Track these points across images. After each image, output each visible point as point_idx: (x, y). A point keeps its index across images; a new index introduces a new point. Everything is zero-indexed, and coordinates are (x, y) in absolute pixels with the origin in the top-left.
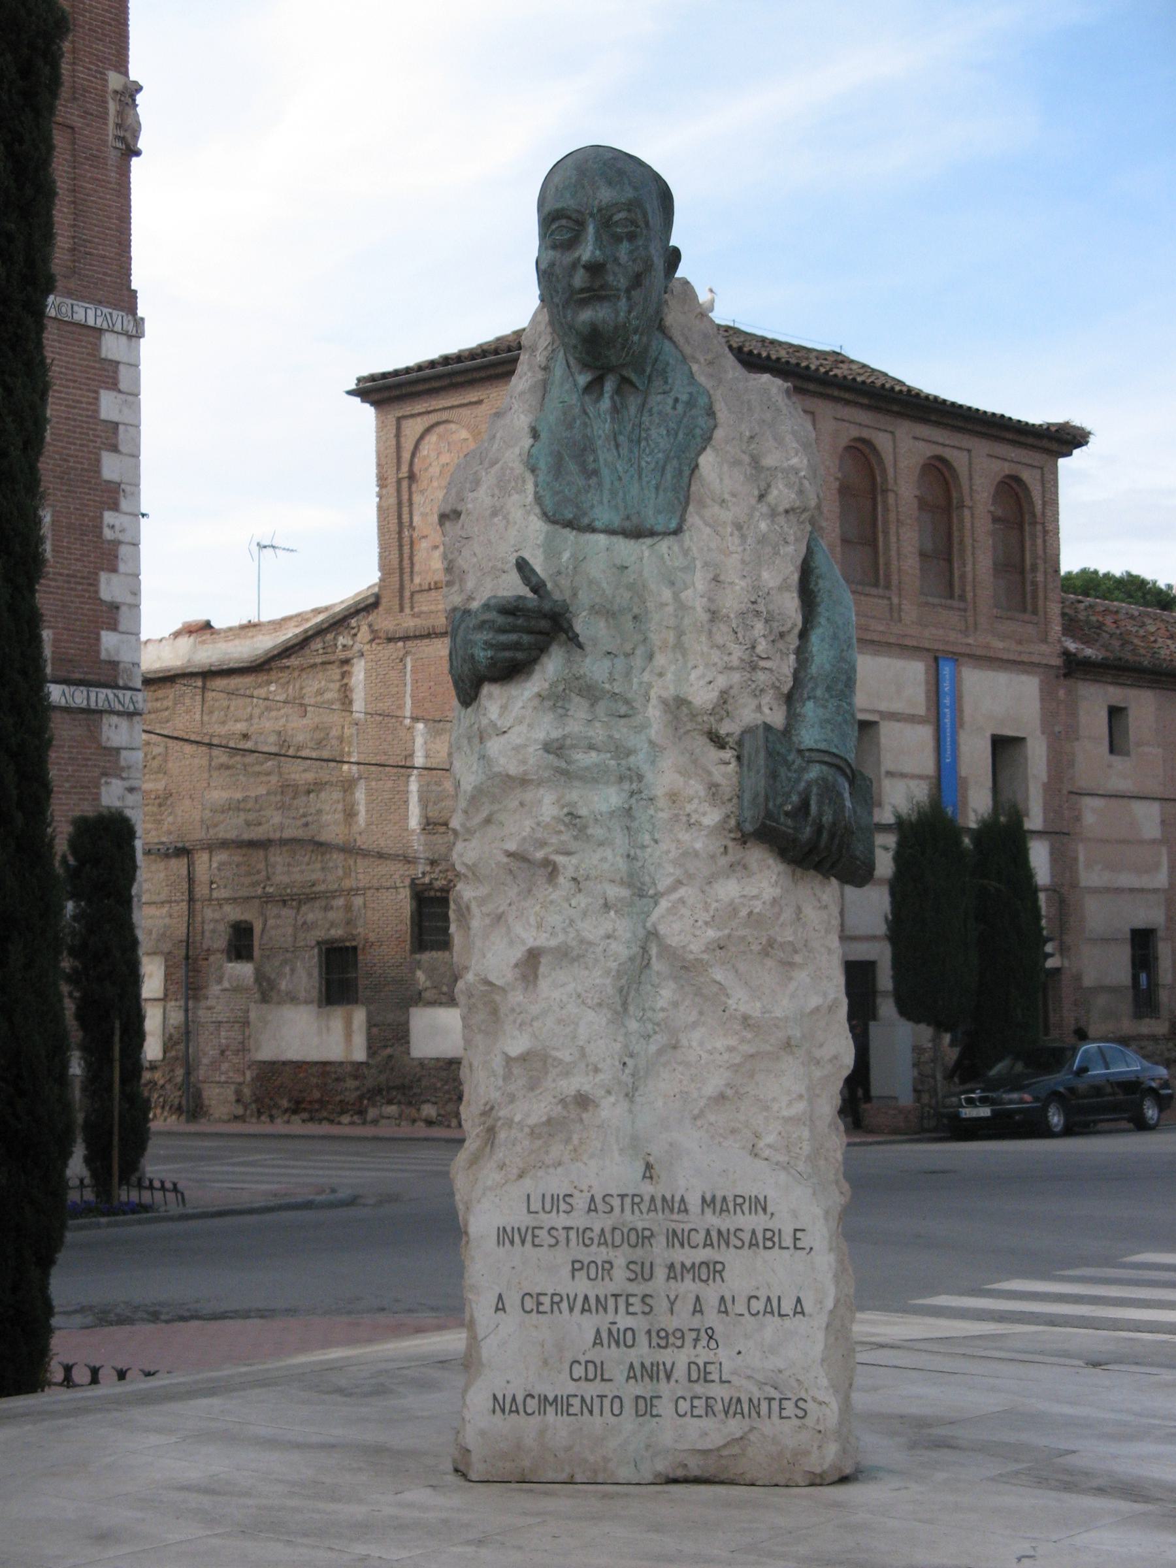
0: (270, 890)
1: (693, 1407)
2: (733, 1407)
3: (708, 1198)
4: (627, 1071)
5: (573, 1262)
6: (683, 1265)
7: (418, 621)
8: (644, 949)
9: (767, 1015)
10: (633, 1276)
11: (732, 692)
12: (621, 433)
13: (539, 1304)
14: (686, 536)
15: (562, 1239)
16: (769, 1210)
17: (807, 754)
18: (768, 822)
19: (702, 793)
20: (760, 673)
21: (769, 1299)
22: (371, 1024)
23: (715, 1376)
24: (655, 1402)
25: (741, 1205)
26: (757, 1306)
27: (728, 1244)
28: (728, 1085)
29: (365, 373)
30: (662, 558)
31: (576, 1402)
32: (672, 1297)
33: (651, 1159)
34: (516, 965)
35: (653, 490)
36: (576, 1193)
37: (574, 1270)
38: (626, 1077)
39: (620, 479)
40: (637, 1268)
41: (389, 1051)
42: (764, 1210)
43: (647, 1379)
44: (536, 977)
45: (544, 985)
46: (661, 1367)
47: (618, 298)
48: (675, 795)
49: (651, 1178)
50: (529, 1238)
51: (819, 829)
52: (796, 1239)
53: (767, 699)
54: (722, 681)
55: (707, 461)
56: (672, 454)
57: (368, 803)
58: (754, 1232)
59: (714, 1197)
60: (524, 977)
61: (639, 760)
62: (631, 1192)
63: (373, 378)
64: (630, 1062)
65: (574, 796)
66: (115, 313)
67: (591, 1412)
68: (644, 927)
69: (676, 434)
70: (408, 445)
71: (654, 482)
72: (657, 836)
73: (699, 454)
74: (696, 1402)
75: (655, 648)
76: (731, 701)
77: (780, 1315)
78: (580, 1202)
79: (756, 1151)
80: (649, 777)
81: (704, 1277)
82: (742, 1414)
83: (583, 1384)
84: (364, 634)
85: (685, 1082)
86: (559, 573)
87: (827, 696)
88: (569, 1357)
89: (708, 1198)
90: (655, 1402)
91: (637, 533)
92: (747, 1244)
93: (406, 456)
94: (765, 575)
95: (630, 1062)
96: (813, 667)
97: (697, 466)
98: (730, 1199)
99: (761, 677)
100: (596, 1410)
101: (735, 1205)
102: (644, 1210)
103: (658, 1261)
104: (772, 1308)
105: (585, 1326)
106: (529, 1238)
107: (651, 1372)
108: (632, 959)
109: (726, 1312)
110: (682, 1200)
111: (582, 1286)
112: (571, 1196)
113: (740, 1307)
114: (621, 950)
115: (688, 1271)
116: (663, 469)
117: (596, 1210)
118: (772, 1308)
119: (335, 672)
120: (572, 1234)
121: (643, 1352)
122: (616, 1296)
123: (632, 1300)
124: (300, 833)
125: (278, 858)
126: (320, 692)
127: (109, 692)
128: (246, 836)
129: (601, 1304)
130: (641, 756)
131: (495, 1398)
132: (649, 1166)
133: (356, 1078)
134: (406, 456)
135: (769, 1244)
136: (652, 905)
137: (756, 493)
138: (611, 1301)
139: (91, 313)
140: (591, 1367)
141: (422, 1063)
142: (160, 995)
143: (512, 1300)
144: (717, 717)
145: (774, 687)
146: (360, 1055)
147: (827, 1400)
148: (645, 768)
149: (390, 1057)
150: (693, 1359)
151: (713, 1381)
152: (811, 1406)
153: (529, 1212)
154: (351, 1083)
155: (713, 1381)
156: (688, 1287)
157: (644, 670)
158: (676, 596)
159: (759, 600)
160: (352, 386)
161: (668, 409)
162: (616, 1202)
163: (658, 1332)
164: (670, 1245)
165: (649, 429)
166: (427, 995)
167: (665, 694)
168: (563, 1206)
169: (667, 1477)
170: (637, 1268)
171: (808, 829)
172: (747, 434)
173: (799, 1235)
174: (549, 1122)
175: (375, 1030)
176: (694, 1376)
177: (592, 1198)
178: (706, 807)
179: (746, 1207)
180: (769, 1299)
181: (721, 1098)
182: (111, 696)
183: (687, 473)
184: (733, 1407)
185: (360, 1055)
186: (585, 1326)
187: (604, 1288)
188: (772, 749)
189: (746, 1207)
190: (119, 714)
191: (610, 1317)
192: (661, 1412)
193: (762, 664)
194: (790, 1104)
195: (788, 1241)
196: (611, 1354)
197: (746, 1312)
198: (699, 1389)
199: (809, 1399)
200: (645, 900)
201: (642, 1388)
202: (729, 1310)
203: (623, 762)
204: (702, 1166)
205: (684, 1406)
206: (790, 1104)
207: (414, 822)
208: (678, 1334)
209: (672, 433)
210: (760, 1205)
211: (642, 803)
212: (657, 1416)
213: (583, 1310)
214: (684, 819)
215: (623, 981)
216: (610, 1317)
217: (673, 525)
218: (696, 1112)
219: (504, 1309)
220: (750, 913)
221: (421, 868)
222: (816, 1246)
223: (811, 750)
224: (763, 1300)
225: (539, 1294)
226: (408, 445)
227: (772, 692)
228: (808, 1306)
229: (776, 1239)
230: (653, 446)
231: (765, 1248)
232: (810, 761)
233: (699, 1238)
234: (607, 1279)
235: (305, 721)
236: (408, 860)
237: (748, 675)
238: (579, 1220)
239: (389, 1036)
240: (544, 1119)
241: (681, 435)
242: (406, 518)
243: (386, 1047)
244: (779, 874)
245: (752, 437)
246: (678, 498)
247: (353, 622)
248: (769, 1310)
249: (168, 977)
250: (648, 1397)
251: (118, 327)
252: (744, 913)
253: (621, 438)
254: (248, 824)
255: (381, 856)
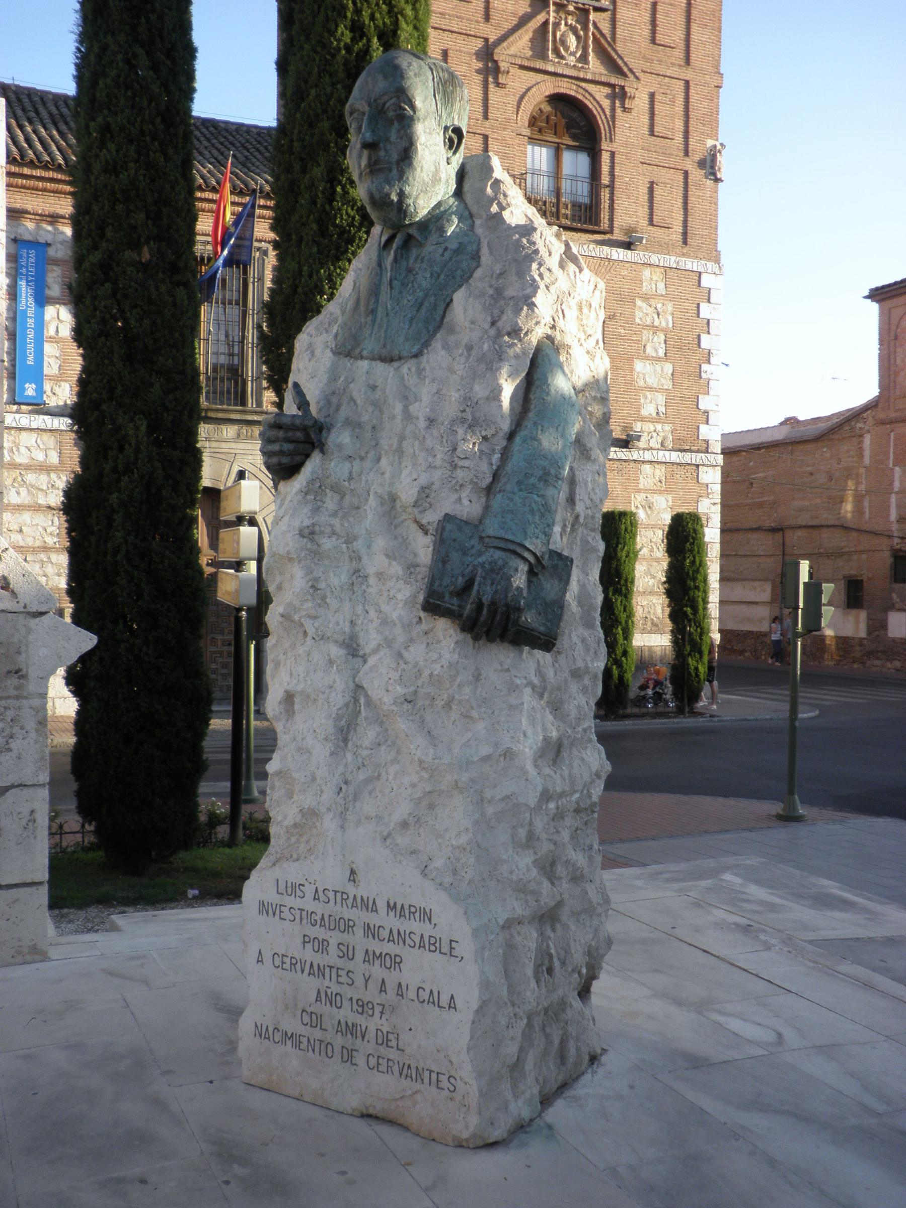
0: (821, 550)
1: (378, 1064)
2: (405, 1071)
3: (392, 905)
4: (341, 795)
5: (304, 936)
6: (374, 953)
7: (898, 414)
8: (356, 700)
9: (436, 761)
10: (341, 955)
11: (434, 487)
12: (396, 279)
13: (283, 963)
14: (424, 359)
15: (298, 917)
16: (433, 922)
17: (487, 540)
18: (431, 601)
19: (401, 573)
20: (459, 471)
21: (431, 991)
22: (869, 619)
23: (393, 1043)
24: (354, 1053)
25: (414, 913)
26: (425, 995)
27: (404, 942)
28: (410, 814)
29: (874, 287)
30: (403, 379)
31: (304, 1040)
32: (367, 976)
33: (354, 866)
34: (280, 703)
35: (407, 323)
36: (306, 884)
37: (304, 942)
38: (340, 800)
39: (387, 315)
40: (344, 949)
41: (877, 633)
42: (430, 920)
43: (349, 1035)
44: (294, 712)
45: (299, 717)
46: (359, 1028)
47: (390, 170)
48: (381, 573)
49: (354, 881)
50: (278, 912)
51: (480, 606)
52: (451, 948)
53: (465, 493)
54: (424, 479)
55: (459, 297)
56: (431, 292)
57: (870, 507)
58: (422, 936)
59: (395, 903)
60: (287, 711)
61: (359, 545)
62: (341, 890)
63: (877, 289)
64: (344, 787)
65: (318, 573)
66: (708, 263)
67: (313, 1050)
68: (354, 682)
69: (439, 276)
70: (894, 321)
71: (409, 316)
72: (367, 607)
73: (454, 292)
74: (381, 1060)
75: (383, 452)
76: (433, 495)
77: (439, 1006)
78: (309, 891)
79: (426, 871)
80: (365, 559)
81: (388, 965)
82: (411, 1077)
83: (308, 1027)
84: (870, 421)
85: (381, 808)
86: (334, 393)
87: (516, 489)
88: (300, 1006)
89: (392, 905)
90: (354, 1053)
91: (388, 359)
92: (417, 945)
93: (893, 327)
94: (477, 388)
95: (344, 787)
96: (510, 465)
97: (452, 300)
98: (406, 907)
99: (460, 474)
100: (317, 1051)
101: (410, 912)
102: (350, 906)
103: (357, 948)
104: (433, 1000)
105: (310, 986)
106: (278, 912)
107: (350, 1029)
108: (347, 705)
109: (402, 996)
110: (374, 902)
111: (308, 955)
112: (303, 885)
113: (412, 994)
114: (339, 699)
115: (378, 958)
116: (421, 305)
117: (319, 899)
118: (433, 1000)
119: (855, 440)
120: (304, 913)
121: (346, 1014)
122: (331, 967)
123: (340, 972)
124: (836, 523)
125: (825, 534)
126: (848, 451)
127: (703, 455)
128: (810, 524)
129: (321, 971)
130: (361, 541)
131: (256, 1026)
132: (353, 872)
133: (860, 645)
134: (893, 327)
135: (433, 948)
136: (361, 663)
137: (489, 319)
138: (327, 970)
139: (695, 264)
140: (314, 1017)
141: (893, 640)
142: (768, 600)
143: (267, 956)
144: (420, 509)
145: (471, 482)
146: (863, 634)
147: (470, 1081)
148: (363, 552)
149: (878, 636)
150: (380, 1027)
151: (392, 1047)
152: (459, 1084)
153: (278, 893)
154: (858, 648)
155: (392, 1047)
156: (377, 972)
157: (371, 470)
158: (406, 409)
159: (467, 409)
160: (867, 293)
161: (437, 256)
162: (331, 895)
163: (358, 1000)
164: (366, 935)
165: (417, 274)
166: (897, 606)
167: (380, 490)
168: (299, 893)
169: (362, 1112)
170: (344, 949)
171: (469, 606)
172: (498, 272)
173: (454, 945)
174: (295, 825)
175: (871, 622)
176: (380, 1041)
177: (317, 891)
178: (401, 584)
179: (417, 915)
180: (431, 991)
181: (404, 825)
182: (704, 457)
183: (442, 307)
184: (405, 1071)
185: (863, 634)
186: (310, 986)
187: (319, 959)
188: (450, 535)
189: (417, 915)
190: (707, 466)
191: (327, 982)
192: (358, 1062)
193: (461, 463)
194: (459, 835)
195: (445, 949)
196: (324, 1009)
197: (415, 999)
198: (383, 1050)
199: (458, 1079)
200: (356, 660)
201: (348, 1041)
202: (405, 995)
203: (350, 546)
204: (391, 878)
205: (373, 1061)
206: (459, 835)
207: (893, 516)
208: (370, 1006)
209: (435, 276)
210: (426, 916)
211: (360, 579)
212: (356, 1064)
213: (310, 974)
214: (385, 594)
215: (343, 723)
216: (327, 982)
217: (415, 350)
218: (385, 834)
219: (262, 961)
220: (431, 675)
221: (896, 540)
222: (466, 957)
223: (489, 537)
224: (428, 991)
225: (283, 955)
226: (894, 321)
227: (470, 486)
228: (459, 1003)
229: (437, 945)
230: (416, 286)
231: (430, 951)
232: (487, 547)
233: (385, 934)
234: (325, 952)
235: (840, 466)
236: (890, 537)
237: (450, 473)
238: (309, 904)
239: (878, 626)
240: (292, 823)
241: (442, 277)
242: (892, 361)
243: (876, 631)
244: (456, 643)
245: (501, 274)
246: (427, 328)
247: (865, 415)
248: (431, 1000)
249: (773, 591)
250: (350, 1049)
251: (709, 271)
252: (426, 673)
253: (395, 283)
254: (812, 518)
255: (876, 534)
